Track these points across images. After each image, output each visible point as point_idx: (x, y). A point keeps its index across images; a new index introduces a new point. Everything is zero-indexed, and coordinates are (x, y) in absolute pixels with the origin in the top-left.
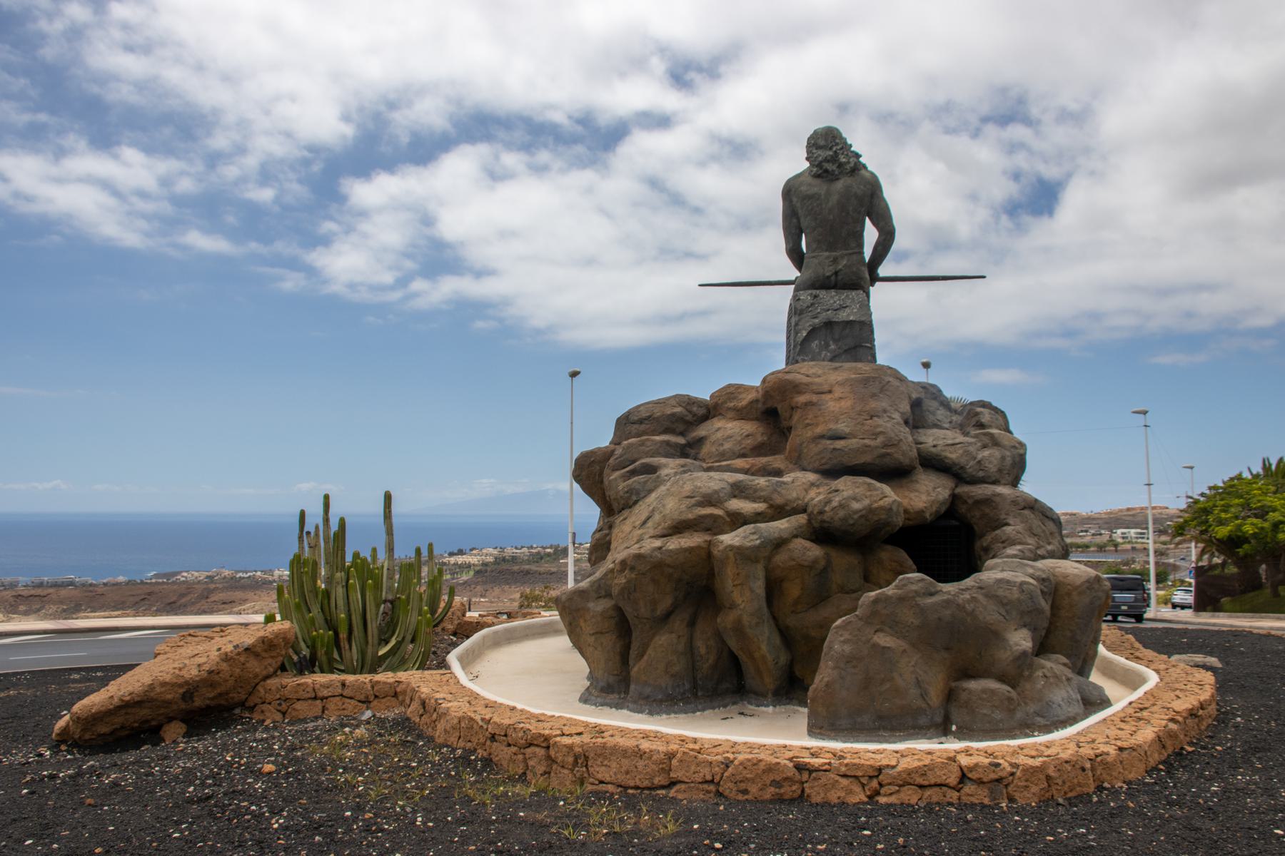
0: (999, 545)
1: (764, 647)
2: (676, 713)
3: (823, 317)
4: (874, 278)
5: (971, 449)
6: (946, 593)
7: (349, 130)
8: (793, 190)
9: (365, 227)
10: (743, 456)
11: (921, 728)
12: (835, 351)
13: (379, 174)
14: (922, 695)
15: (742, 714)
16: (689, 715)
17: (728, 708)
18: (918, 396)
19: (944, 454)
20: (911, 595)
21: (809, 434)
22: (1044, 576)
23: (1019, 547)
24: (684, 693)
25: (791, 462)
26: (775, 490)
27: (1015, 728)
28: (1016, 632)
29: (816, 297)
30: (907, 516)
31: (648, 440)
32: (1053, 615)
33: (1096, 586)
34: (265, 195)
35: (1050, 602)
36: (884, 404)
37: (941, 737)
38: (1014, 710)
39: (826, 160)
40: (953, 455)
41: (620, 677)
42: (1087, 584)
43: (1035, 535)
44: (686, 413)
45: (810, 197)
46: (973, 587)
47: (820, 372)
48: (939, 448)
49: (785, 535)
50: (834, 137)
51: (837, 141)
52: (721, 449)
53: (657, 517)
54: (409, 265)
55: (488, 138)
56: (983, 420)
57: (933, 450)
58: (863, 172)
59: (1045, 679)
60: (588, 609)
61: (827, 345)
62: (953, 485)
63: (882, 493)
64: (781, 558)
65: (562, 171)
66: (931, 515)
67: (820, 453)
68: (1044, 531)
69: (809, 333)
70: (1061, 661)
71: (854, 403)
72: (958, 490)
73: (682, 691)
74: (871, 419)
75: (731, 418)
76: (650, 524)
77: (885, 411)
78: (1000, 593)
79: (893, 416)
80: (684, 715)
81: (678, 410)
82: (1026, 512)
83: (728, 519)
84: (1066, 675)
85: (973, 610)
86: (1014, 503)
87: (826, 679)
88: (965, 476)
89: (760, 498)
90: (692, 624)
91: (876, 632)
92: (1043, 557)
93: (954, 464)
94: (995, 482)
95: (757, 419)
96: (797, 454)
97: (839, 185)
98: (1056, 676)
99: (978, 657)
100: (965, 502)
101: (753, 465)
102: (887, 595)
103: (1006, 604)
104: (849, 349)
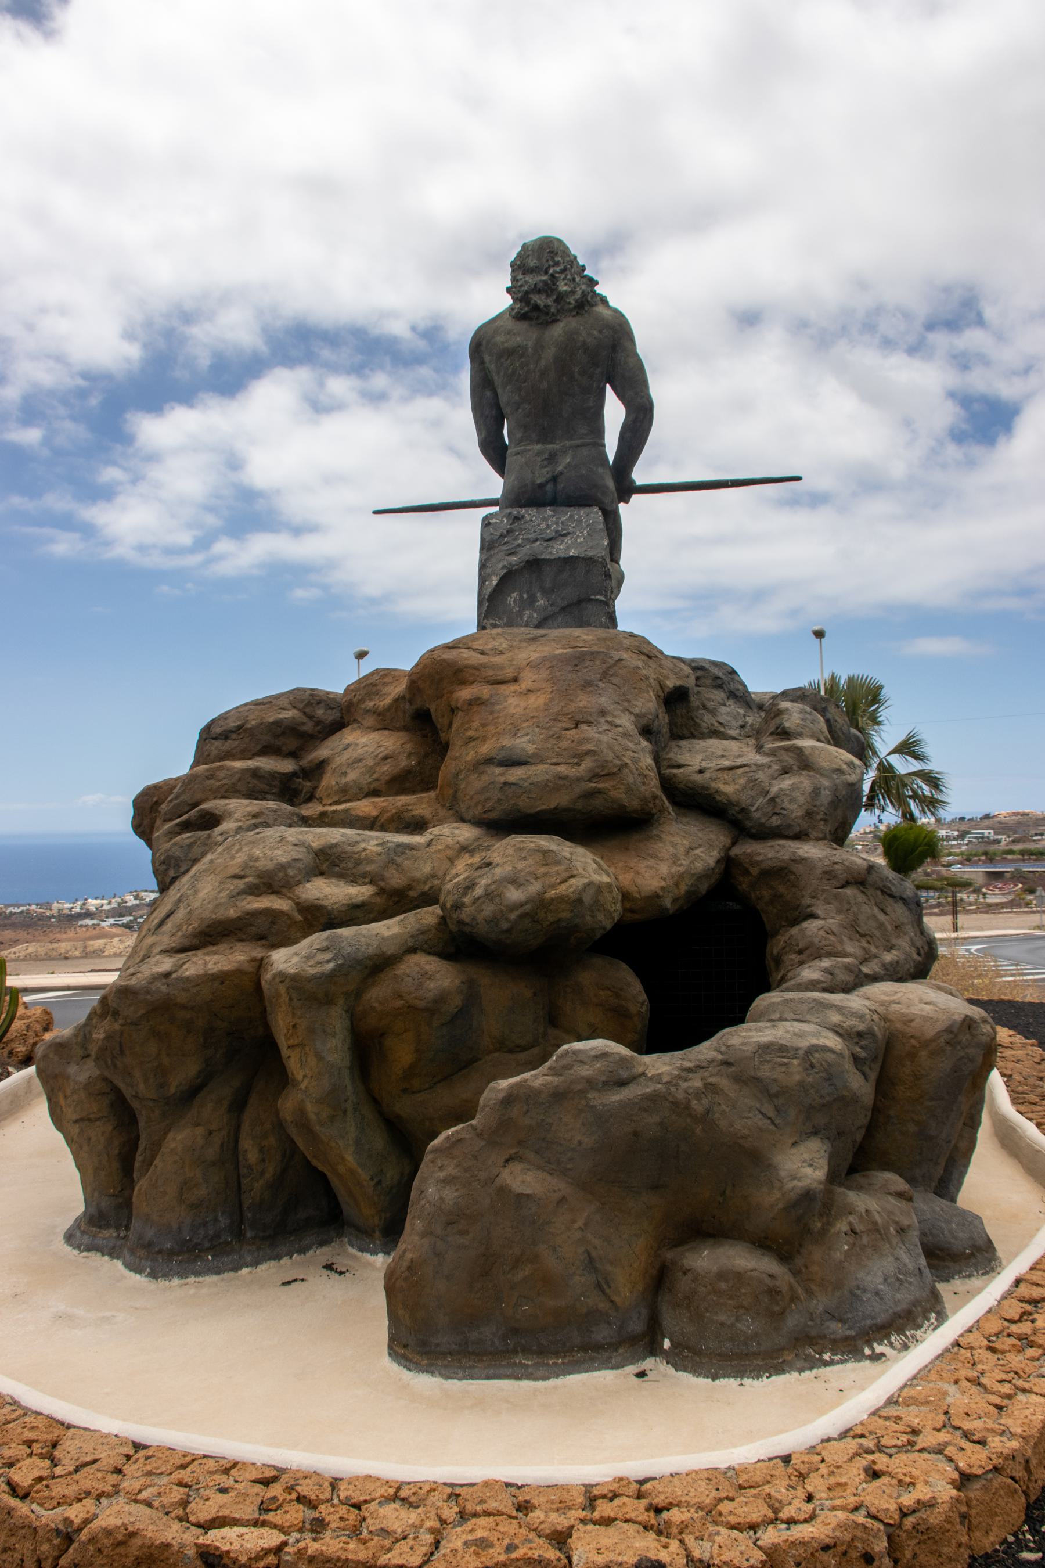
0: (793, 956)
1: (350, 1158)
2: (198, 1274)
3: (525, 553)
4: (627, 490)
5: (761, 775)
6: (652, 1078)
7: (134, 352)
8: (484, 342)
9: (155, 473)
10: (375, 793)
11: (598, 1348)
12: (545, 609)
13: (173, 408)
14: (599, 1285)
15: (329, 1267)
16: (226, 1275)
17: (311, 1252)
18: (678, 683)
19: (713, 785)
20: (579, 1087)
21: (470, 756)
22: (861, 1027)
23: (826, 963)
24: (217, 1236)
25: (443, 806)
26: (392, 861)
27: (783, 1349)
28: (794, 1151)
29: (517, 519)
30: (628, 905)
31: (221, 768)
32: (876, 1109)
33: (964, 1038)
34: (31, 436)
35: (873, 1076)
36: (604, 699)
37: (644, 1359)
38: (783, 1313)
39: (536, 290)
40: (728, 788)
41: (120, 1200)
42: (946, 1037)
43: (862, 936)
44: (305, 719)
45: (510, 353)
46: (712, 1061)
47: (504, 645)
48: (707, 775)
49: (390, 950)
50: (553, 253)
51: (557, 259)
52: (344, 780)
53: (181, 914)
54: (211, 520)
55: (308, 358)
56: (787, 724)
57: (698, 778)
58: (600, 309)
59: (851, 1239)
60: (68, 1078)
61: (533, 600)
62: (728, 842)
63: (568, 869)
64: (378, 994)
65: (405, 400)
66: (675, 900)
67: (484, 789)
68: (881, 926)
69: (503, 580)
70: (893, 1188)
71: (552, 700)
72: (736, 851)
73: (211, 1232)
74: (576, 727)
75: (369, 728)
76: (168, 927)
77: (603, 713)
78: (765, 1072)
79: (618, 722)
80: (215, 1278)
81: (290, 714)
82: (849, 891)
83: (299, 918)
84: (897, 1223)
85: (708, 1112)
86: (829, 874)
87: (409, 1256)
88: (748, 824)
89: (364, 875)
90: (238, 1105)
91: (507, 1161)
92: (874, 979)
93: (730, 803)
94: (800, 836)
95: (405, 728)
96: (451, 792)
97: (557, 331)
98: (875, 1229)
99: (721, 1199)
100: (747, 872)
101: (383, 811)
102: (531, 1089)
103: (776, 1095)
104: (569, 606)
